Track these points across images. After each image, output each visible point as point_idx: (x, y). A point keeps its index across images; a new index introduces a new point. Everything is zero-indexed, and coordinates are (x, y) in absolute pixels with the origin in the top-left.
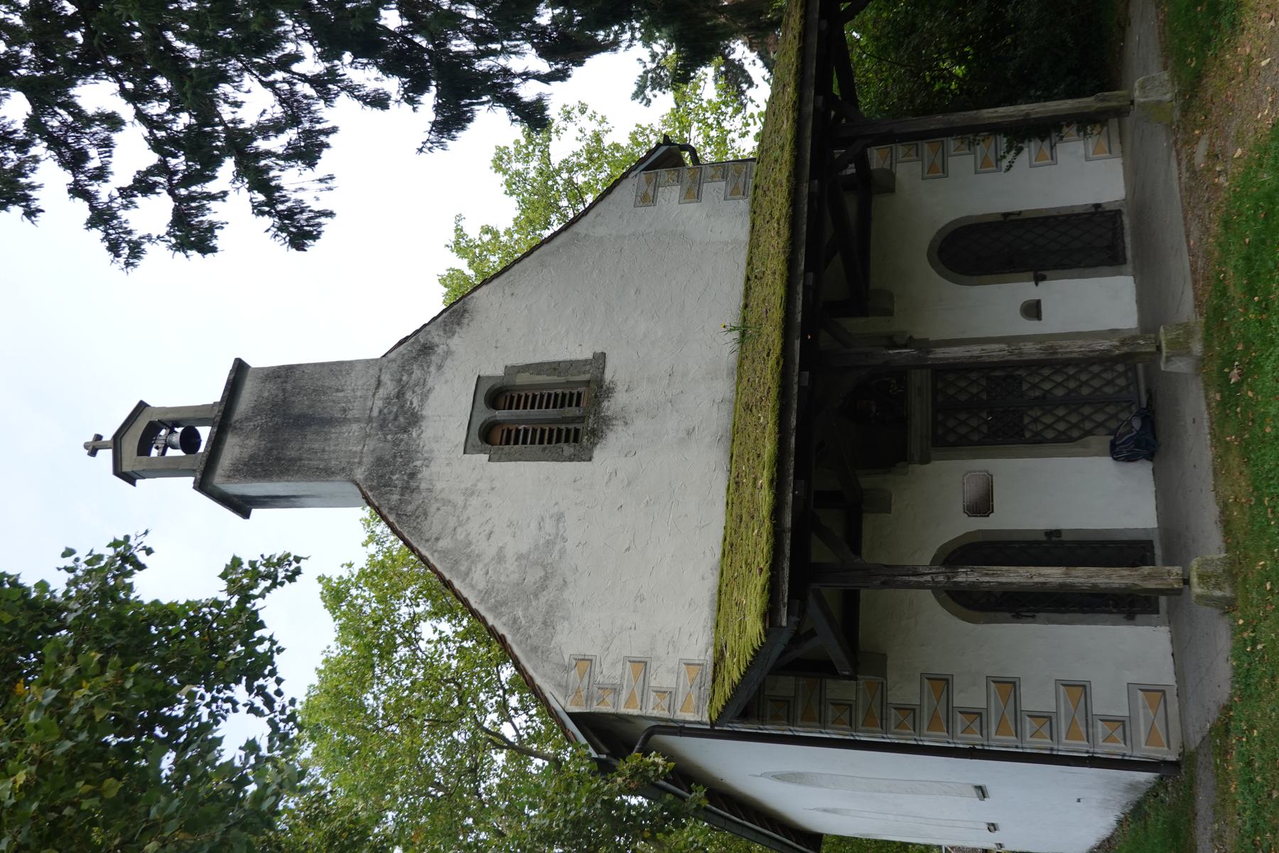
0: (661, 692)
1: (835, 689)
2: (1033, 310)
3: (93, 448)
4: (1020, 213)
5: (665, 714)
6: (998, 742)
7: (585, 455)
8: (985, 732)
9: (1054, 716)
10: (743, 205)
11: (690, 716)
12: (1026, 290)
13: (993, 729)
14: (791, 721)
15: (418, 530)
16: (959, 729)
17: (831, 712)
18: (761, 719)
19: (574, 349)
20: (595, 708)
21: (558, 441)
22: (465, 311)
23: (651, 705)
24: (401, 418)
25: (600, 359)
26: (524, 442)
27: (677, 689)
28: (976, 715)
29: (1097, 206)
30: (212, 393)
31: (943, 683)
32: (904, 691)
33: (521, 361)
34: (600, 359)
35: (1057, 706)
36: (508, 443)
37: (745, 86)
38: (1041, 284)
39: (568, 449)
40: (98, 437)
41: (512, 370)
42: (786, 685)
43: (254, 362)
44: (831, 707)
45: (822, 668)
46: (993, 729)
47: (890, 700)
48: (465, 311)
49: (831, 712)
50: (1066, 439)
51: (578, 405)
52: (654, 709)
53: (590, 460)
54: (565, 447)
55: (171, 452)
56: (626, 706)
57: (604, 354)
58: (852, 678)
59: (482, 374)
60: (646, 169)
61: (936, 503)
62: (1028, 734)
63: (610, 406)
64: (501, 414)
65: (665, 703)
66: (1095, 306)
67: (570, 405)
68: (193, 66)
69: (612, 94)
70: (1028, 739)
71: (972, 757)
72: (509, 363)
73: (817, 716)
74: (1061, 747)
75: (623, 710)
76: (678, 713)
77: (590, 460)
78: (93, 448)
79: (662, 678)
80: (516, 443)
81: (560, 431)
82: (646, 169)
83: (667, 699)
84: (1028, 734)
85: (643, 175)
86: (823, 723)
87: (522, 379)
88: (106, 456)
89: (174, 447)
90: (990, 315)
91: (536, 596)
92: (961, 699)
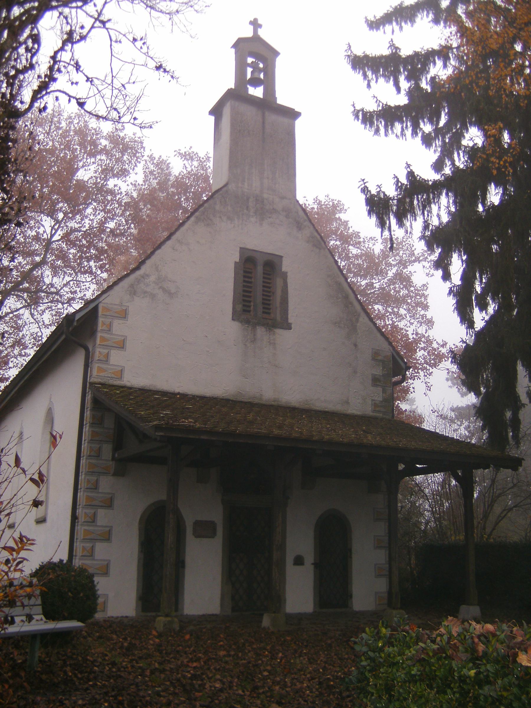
0: (107, 355)
1: (107, 450)
2: (299, 561)
3: (255, 24)
4: (351, 557)
5: (96, 357)
6: (80, 529)
7: (235, 316)
8: (85, 524)
9: (93, 524)
10: (368, 410)
11: (95, 373)
12: (309, 559)
13: (86, 528)
14: (92, 425)
15: (198, 220)
16: (87, 511)
17: (96, 446)
18: (93, 409)
19: (295, 312)
20: (101, 320)
21: (244, 300)
22: (320, 249)
23: (101, 350)
24: (262, 209)
25: (288, 327)
26: (244, 281)
27: (112, 334)
28: (93, 520)
29: (351, 596)
30: (283, 98)
31: (109, 504)
32: (107, 484)
33: (289, 281)
34: (288, 327)
35: (97, 560)
36: (245, 272)
37: (420, 116)
38: (313, 566)
39: (239, 307)
40: (260, 26)
41: (284, 276)
42: (109, 423)
43: (299, 123)
44: (96, 478)
45: (118, 444)
46: (86, 528)
47: (97, 544)
48: (320, 249)
49: (96, 446)
50: (230, 575)
51: (264, 312)
52: (98, 352)
53: (233, 320)
54: (241, 306)
55: (249, 70)
56: (101, 337)
57: (290, 329)
58: (113, 459)
59: (284, 259)
60: (393, 357)
61: (202, 504)
62: (84, 545)
63: (260, 331)
64: (260, 269)
65: (102, 358)
66: (299, 594)
67: (264, 308)
68: (508, 414)
69: (438, 312)
70: (82, 545)
71: (76, 472)
72: (289, 274)
73: (87, 537)
74: (78, 544)
75: (99, 335)
76: (97, 365)
77: (233, 320)
78: (255, 24)
79: (117, 358)
80: (244, 277)
81: (250, 302)
82: (393, 357)
83: (104, 359)
84: (84, 545)
85: (389, 354)
86: (91, 441)
87: (279, 282)
88: (249, 33)
89: (252, 72)
90: (299, 539)
91: (161, 287)
92: (101, 513)
